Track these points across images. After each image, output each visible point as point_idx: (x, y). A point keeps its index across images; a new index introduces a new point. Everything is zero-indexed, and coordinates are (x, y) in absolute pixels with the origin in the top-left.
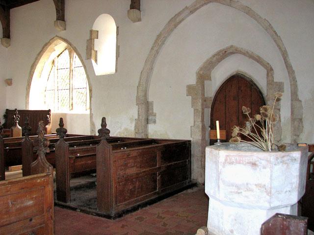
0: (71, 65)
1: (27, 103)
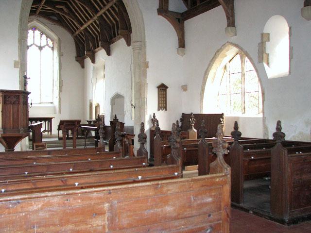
0: (243, 69)
1: (201, 107)
